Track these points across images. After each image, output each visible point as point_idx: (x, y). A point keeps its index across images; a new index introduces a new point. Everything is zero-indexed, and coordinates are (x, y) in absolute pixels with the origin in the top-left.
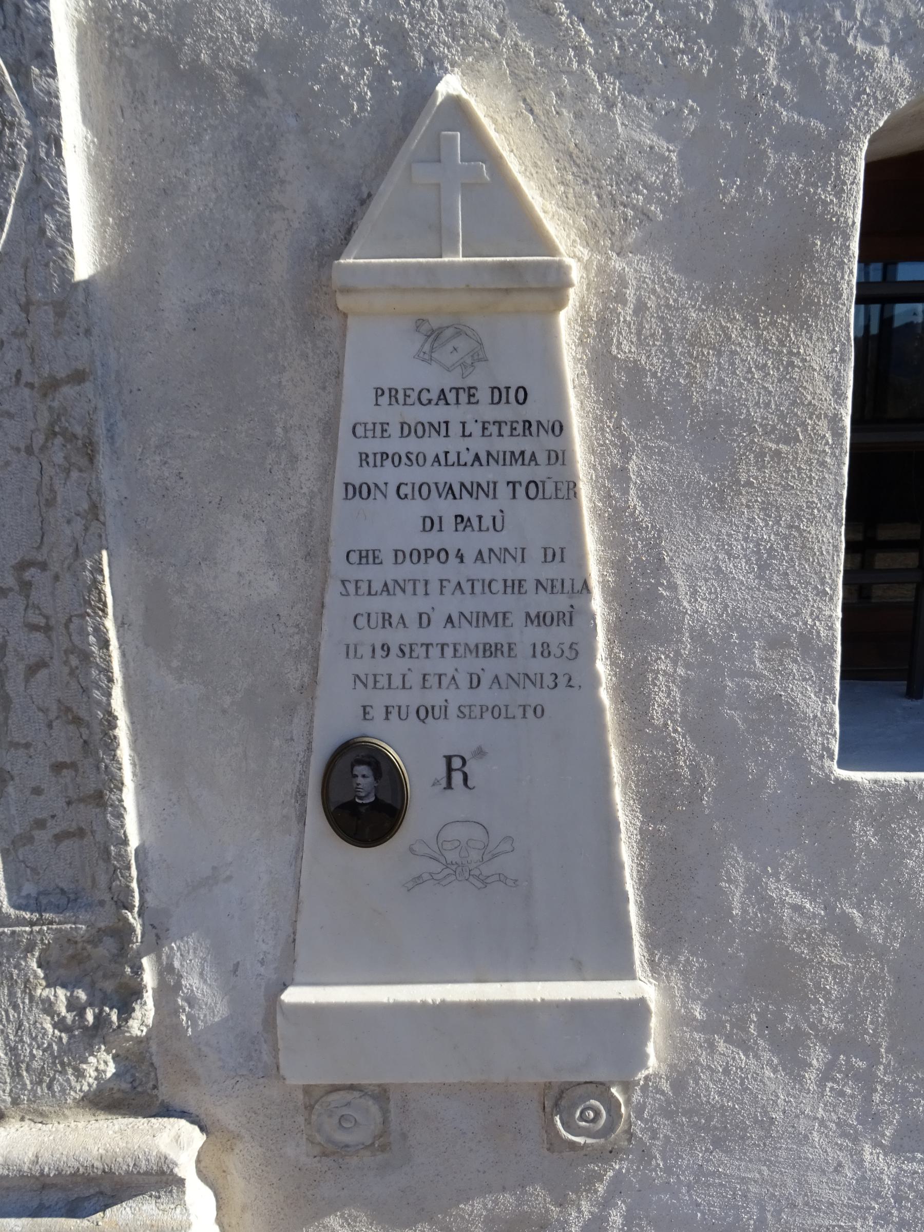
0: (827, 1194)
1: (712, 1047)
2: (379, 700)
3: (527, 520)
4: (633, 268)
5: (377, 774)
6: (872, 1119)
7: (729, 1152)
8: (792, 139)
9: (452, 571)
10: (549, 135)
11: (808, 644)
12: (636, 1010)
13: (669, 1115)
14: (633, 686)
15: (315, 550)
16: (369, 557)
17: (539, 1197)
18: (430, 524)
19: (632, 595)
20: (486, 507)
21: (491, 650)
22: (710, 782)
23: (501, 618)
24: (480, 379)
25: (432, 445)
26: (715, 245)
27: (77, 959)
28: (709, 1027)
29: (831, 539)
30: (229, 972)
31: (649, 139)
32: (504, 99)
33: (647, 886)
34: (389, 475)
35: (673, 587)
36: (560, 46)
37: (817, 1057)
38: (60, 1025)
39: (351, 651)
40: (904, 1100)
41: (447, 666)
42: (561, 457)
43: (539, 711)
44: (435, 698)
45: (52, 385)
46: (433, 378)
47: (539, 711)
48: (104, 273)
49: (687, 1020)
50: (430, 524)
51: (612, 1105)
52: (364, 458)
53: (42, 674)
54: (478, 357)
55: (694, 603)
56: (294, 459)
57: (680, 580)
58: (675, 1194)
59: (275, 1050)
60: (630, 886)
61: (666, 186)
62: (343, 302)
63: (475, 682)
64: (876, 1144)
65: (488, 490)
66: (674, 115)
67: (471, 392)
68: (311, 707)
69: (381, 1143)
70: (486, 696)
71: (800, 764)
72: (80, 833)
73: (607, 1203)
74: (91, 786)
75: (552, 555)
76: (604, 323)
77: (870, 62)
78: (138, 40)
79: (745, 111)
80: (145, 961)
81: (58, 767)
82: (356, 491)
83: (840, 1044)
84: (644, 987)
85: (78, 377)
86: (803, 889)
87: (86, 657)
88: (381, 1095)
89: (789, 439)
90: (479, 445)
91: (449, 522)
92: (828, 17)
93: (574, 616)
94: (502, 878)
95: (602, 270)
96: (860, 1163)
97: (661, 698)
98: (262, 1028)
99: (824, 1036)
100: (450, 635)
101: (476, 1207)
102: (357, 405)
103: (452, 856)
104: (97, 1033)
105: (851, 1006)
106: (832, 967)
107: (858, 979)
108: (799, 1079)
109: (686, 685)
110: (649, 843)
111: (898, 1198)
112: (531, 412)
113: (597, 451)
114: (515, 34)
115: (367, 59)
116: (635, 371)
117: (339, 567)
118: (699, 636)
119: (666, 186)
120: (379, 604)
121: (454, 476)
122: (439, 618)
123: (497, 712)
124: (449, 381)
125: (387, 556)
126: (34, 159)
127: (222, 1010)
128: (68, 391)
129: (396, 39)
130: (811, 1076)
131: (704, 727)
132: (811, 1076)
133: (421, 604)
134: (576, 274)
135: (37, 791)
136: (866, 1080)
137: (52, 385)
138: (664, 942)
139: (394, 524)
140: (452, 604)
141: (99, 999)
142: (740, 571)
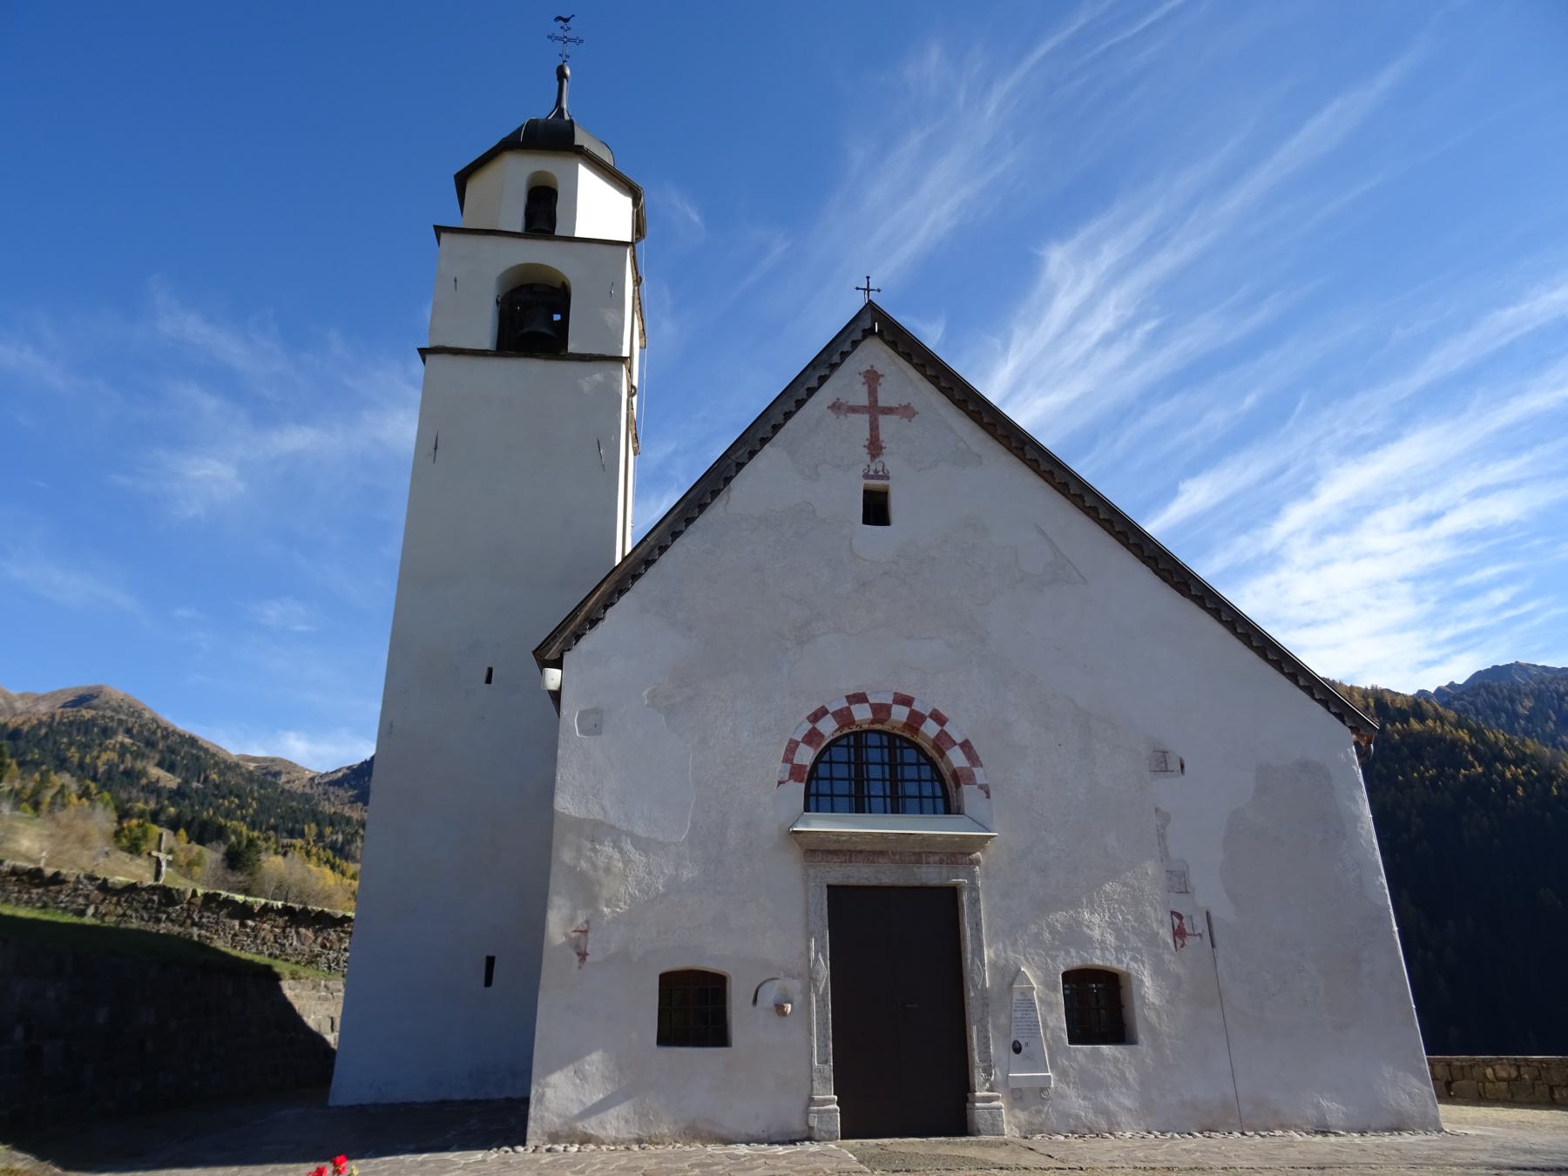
19: (1044, 1022)
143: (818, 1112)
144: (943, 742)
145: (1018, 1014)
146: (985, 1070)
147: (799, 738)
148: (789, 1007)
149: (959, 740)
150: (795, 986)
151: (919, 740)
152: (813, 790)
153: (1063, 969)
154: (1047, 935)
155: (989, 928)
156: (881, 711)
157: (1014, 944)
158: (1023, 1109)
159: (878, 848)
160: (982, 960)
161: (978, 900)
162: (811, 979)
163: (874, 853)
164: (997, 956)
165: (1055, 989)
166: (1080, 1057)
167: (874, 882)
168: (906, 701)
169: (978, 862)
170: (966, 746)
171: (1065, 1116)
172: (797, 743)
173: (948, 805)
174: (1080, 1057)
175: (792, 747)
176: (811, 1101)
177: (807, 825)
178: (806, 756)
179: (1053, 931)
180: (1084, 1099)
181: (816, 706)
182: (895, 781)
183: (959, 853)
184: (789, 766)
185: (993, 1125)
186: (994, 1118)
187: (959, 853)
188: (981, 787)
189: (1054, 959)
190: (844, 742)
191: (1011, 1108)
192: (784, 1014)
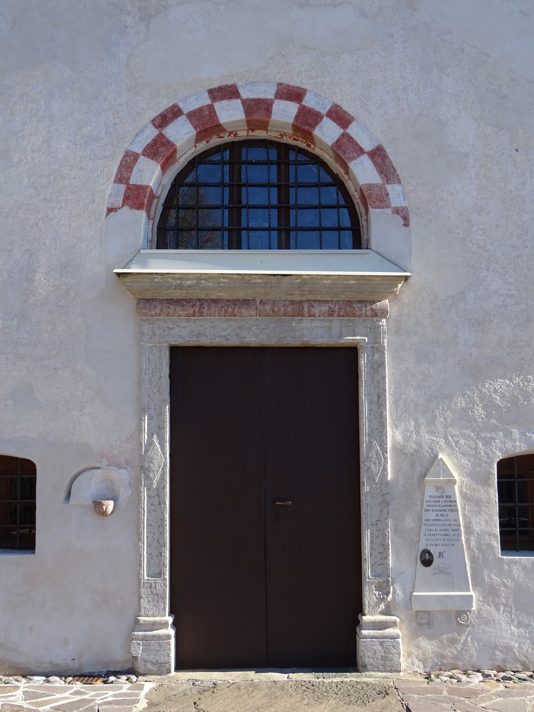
0: (506, 635)
1: (484, 605)
2: (429, 543)
3: (451, 515)
4: (465, 480)
5: (429, 555)
6: (512, 621)
7: (488, 626)
8: (486, 462)
9: (440, 522)
10: (453, 462)
11: (494, 535)
12: (471, 596)
13: (477, 618)
14: (468, 541)
15: (420, 518)
16: (428, 520)
17: (456, 635)
18: (437, 515)
19: (468, 527)
20: (445, 513)
21: (446, 535)
22: (481, 558)
23: (448, 530)
24: (444, 495)
25: (437, 504)
26: (477, 477)
27: (380, 586)
28: (483, 602)
29: (496, 519)
30: (404, 590)
31: (466, 462)
32: (447, 457)
33: (471, 575)
34: (431, 508)
35: (473, 526)
36: (454, 450)
37: (502, 608)
38: (377, 598)
39: (425, 535)
40: (517, 617)
41: (440, 537)
42: (456, 506)
43: (454, 545)
44: (438, 542)
45: (384, 494)
46: (438, 494)
47: (454, 545)
48: (391, 479)
49: (479, 600)
50: (437, 515)
51: (468, 616)
52: (427, 506)
53: (378, 538)
54: (444, 492)
55: (477, 528)
56: (417, 505)
57: (474, 525)
58: (479, 635)
59: (411, 604)
60: (469, 575)
61: (469, 468)
62: (425, 484)
63: (444, 540)
64: (514, 626)
65: (446, 511)
66: (470, 459)
67: (443, 496)
68: (419, 544)
69: (429, 623)
70: (445, 542)
71: (495, 554)
72: (382, 564)
73: (467, 636)
74: (385, 556)
75: (455, 520)
76: (461, 487)
77: (496, 453)
78: (398, 449)
79: (479, 459)
80: (391, 587)
81: (380, 553)
82: (427, 510)
83: (506, 605)
84: (472, 593)
85: (388, 494)
86: (497, 576)
87: (386, 535)
88: (428, 613)
89: (489, 504)
90: (444, 504)
91: (440, 515)
92: (490, 447)
93: (458, 530)
94: (448, 573)
95: (461, 480)
96: (511, 629)
97: (472, 543)
98: (410, 599)
99: (503, 604)
100: (440, 533)
101: (445, 637)
102: (426, 498)
103: (440, 569)
104: (383, 600)
105: (507, 598)
106: (503, 591)
107: (507, 593)
108: (499, 612)
109: (476, 541)
110: (471, 567)
111: (519, 637)
112: (451, 499)
113: (461, 505)
114: (448, 449)
115: (428, 452)
116: (466, 494)
117: (423, 522)
118: (477, 533)
119: (469, 468)
120: (429, 528)
121: (441, 508)
122: (438, 530)
123: (447, 545)
124: (440, 495)
125: (431, 520)
126: (384, 465)
127: (403, 597)
128: (386, 496)
129: (432, 450)
130: (501, 612)
131: (479, 548)
132: (501, 612)
133: (436, 528)
134: (458, 481)
135: (376, 557)
136: (510, 613)
137: (384, 494)
138: (475, 585)
139: (432, 515)
140: (440, 528)
141: (383, 594)
142: (483, 523)
143: (144, 638)
144: (346, 147)
145: (432, 515)
146: (379, 587)
147: (138, 148)
148: (110, 505)
149: (367, 145)
150: (122, 477)
151: (317, 151)
152: (172, 221)
153: (500, 456)
154: (479, 411)
155: (396, 402)
156: (259, 111)
157: (431, 422)
158: (430, 638)
159: (241, 295)
160: (383, 445)
161: (382, 364)
162: (143, 469)
163: (235, 302)
164: (406, 439)
165: (486, 483)
166: (516, 571)
167: (234, 342)
168: (294, 94)
169: (384, 313)
170: (378, 155)
171: (491, 647)
172: (135, 157)
173: (356, 237)
174: (516, 571)
175: (129, 161)
176: (136, 625)
177: (145, 266)
178: (152, 176)
179: (489, 405)
180: (520, 625)
181: (164, 105)
182: (284, 209)
183: (358, 301)
184: (122, 188)
185: (385, 658)
186: (387, 651)
187: (358, 301)
188: (397, 211)
189: (487, 442)
190: (217, 157)
191: (414, 635)
192: (104, 513)
